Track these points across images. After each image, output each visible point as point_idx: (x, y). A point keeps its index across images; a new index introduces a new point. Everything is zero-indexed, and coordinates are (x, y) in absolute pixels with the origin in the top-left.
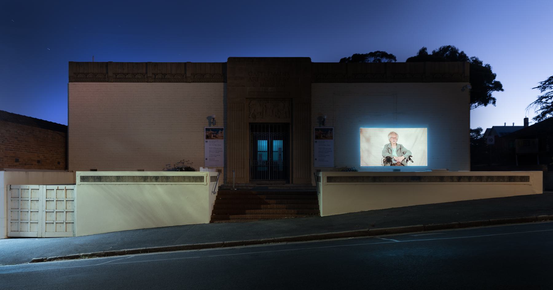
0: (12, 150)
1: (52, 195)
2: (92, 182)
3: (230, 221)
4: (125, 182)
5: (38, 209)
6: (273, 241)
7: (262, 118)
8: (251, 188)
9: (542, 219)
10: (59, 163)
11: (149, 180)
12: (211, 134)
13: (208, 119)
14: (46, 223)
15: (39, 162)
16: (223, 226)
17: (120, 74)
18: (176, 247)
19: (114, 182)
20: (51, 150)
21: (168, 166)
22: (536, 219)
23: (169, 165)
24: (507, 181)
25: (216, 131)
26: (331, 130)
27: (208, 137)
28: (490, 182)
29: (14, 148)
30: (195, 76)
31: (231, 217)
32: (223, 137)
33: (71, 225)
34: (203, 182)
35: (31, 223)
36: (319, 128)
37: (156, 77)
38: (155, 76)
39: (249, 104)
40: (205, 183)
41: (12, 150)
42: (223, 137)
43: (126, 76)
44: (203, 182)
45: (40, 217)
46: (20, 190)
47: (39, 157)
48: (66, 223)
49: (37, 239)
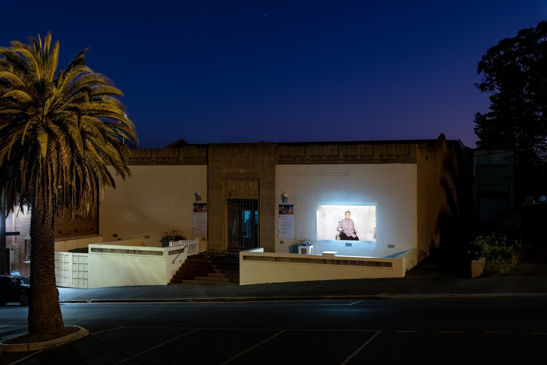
0: (57, 226)
1: (76, 259)
2: (97, 252)
3: (182, 284)
4: (116, 253)
5: (68, 269)
6: (172, 301)
7: (236, 195)
8: (224, 255)
9: (329, 298)
10: (92, 229)
11: (130, 252)
12: (198, 207)
13: (196, 196)
14: (73, 278)
15: (76, 231)
16: (177, 286)
17: (133, 158)
18: (134, 300)
19: (110, 252)
20: (85, 221)
21: (166, 234)
22: (325, 298)
23: (167, 233)
24: (375, 266)
25: (202, 205)
26: (292, 206)
27: (195, 211)
28: (361, 265)
29: (58, 225)
30: (186, 159)
31: (183, 281)
32: (206, 210)
33: (86, 280)
34: (163, 255)
35: (64, 277)
36: (282, 204)
37: (158, 161)
38: (158, 160)
39: (226, 183)
40: (164, 256)
41: (57, 226)
42: (206, 210)
43: (137, 160)
44: (163, 255)
45: (69, 274)
46: (59, 256)
47: (76, 227)
48: (78, 279)
49: (67, 289)
